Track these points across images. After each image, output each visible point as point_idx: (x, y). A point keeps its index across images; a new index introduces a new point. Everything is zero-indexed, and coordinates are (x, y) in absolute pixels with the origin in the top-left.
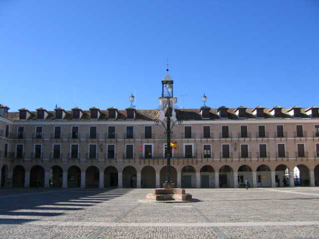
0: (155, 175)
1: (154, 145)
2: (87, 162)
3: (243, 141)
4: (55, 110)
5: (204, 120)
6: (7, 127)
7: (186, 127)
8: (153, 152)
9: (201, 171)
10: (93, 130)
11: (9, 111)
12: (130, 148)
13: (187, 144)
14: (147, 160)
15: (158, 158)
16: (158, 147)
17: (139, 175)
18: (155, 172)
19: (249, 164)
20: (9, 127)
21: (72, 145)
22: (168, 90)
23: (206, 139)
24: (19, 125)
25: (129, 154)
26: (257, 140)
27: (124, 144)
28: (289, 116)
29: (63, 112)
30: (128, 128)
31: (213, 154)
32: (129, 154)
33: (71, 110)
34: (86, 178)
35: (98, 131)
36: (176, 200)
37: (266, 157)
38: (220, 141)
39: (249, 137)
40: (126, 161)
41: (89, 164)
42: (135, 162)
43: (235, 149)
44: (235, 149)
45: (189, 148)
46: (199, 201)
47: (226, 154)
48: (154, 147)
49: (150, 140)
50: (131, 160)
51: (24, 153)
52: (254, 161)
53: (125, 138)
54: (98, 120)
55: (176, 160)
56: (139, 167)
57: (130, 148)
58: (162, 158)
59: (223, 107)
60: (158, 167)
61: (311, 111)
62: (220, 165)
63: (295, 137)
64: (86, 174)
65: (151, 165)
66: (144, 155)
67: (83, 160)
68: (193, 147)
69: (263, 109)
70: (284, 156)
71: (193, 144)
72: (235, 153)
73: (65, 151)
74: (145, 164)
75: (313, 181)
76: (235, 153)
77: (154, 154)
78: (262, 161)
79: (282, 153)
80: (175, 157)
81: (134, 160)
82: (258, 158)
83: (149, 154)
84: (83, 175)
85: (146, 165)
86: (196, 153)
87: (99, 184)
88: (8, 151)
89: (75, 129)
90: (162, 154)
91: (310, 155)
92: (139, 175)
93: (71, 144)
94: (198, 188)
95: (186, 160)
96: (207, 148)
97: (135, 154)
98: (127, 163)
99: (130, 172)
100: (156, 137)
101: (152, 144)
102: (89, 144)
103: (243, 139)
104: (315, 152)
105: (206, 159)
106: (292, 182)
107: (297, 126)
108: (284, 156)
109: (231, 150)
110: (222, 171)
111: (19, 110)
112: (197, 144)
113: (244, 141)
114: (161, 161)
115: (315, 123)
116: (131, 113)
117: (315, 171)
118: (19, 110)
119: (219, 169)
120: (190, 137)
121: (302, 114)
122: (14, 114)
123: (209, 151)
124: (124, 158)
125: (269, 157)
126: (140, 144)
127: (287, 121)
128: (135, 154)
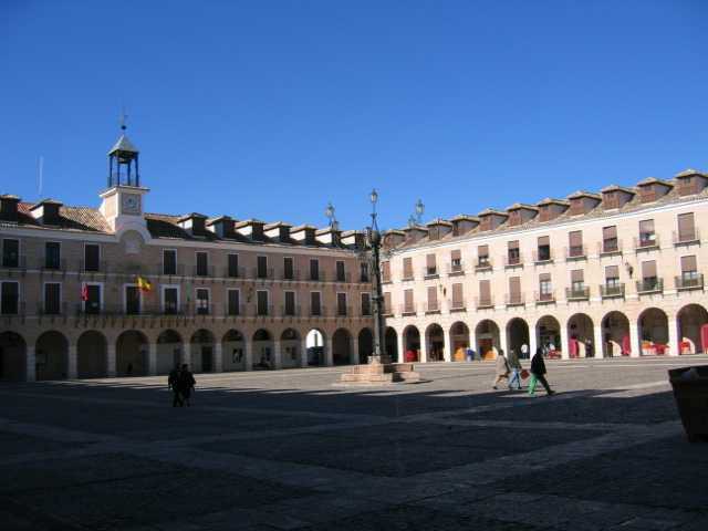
0: (67, 351)
2: (40, 322)
3: (234, 284)
5: (196, 240)
8: (102, 301)
9: (224, 340)
12: (53, 292)
13: (168, 287)
14: (91, 319)
15: (112, 313)
17: (73, 351)
23: (201, 279)
25: (52, 305)
26: (307, 285)
27: (41, 282)
28: (33, 221)
30: (166, 253)
31: (213, 306)
32: (52, 305)
35: (240, 264)
36: (407, 381)
38: (224, 282)
39: (102, 272)
40: (46, 319)
42: (65, 322)
43: (249, 298)
44: (249, 298)
46: (429, 382)
47: (234, 309)
48: (105, 291)
50: (57, 318)
53: (42, 269)
55: (149, 318)
56: (73, 333)
57: (53, 292)
58: (121, 313)
60: (112, 333)
61: (42, 208)
63: (225, 277)
65: (99, 329)
66: (84, 308)
68: (102, 289)
69: (18, 201)
70: (345, 314)
71: (178, 287)
72: (249, 306)
74: (85, 325)
76: (249, 306)
77: (105, 305)
79: (290, 309)
80: (147, 313)
81: (62, 319)
82: (226, 315)
83: (95, 305)
85: (89, 328)
86: (188, 306)
90: (122, 305)
91: (330, 312)
92: (73, 351)
94: (279, 369)
95: (168, 318)
96: (202, 295)
98: (47, 325)
100: (110, 268)
101: (102, 285)
103: (260, 281)
105: (201, 317)
106: (305, 358)
107: (199, 254)
109: (241, 300)
110: (163, 340)
112: (185, 286)
113: (263, 284)
114: (119, 319)
115: (311, 256)
119: (189, 337)
121: (20, 214)
123: (205, 301)
124: (40, 313)
125: (213, 314)
126: (73, 285)
127: (325, 252)
128: (65, 304)
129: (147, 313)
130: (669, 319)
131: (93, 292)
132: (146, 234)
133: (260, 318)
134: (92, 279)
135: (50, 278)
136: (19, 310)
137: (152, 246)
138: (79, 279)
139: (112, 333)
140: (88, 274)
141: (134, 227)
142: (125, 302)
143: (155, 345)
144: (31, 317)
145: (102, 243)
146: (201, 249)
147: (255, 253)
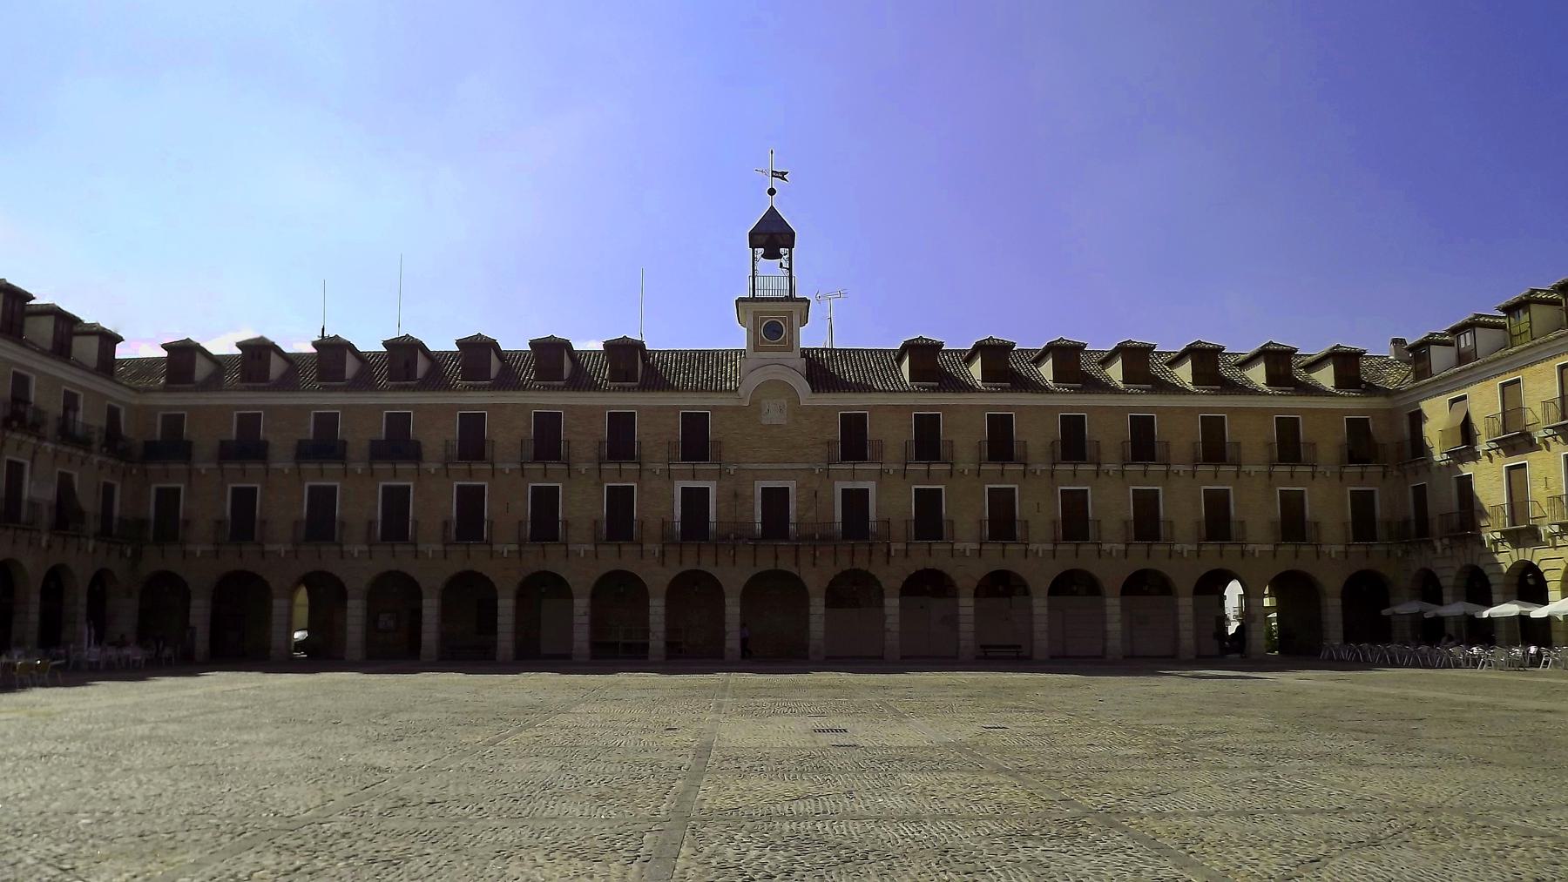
0: (723, 606)
1: (719, 488)
3: (1072, 477)
4: (315, 344)
6: (113, 414)
7: (165, 417)
10: (621, 423)
11: (121, 352)
12: (620, 500)
13: (849, 485)
15: (735, 538)
16: (736, 495)
18: (722, 597)
19: (1096, 568)
20: (123, 414)
21: (459, 487)
22: (771, 277)
24: (610, 407)
29: (349, 356)
30: (846, 419)
33: (309, 349)
34: (668, 616)
37: (1086, 538)
41: (456, 565)
45: (855, 501)
49: (701, 466)
50: (1011, 547)
51: (187, 523)
52: (1111, 555)
54: (492, 388)
56: (658, 576)
59: (262, 339)
62: (980, 570)
64: (667, 606)
65: (706, 565)
67: (431, 548)
68: (1377, 496)
70: (1011, 536)
71: (871, 486)
73: (508, 507)
75: (732, 642)
78: (997, 558)
84: (430, 608)
85: (689, 565)
87: (495, 644)
88: (117, 511)
89: (472, 424)
93: (381, 485)
97: (566, 523)
98: (611, 559)
99: (472, 595)
101: (712, 487)
102: (455, 484)
104: (1198, 523)
108: (1011, 536)
111: (239, 345)
116: (626, 358)
117: (1343, 598)
118: (239, 345)
120: (704, 457)
122: (143, 367)
126: (662, 495)
128: (491, 523)
129: (798, 539)
130: (1494, 588)
131: (695, 500)
132: (803, 387)
133: (1068, 548)
134: (854, 476)
135: (1210, 479)
136: (1018, 533)
137: (815, 408)
138: (670, 476)
139: (733, 576)
140: (687, 466)
141: (774, 373)
142: (759, 519)
143: (896, 602)
144: (356, 548)
145: (714, 408)
146: (998, 407)
147: (452, 408)
